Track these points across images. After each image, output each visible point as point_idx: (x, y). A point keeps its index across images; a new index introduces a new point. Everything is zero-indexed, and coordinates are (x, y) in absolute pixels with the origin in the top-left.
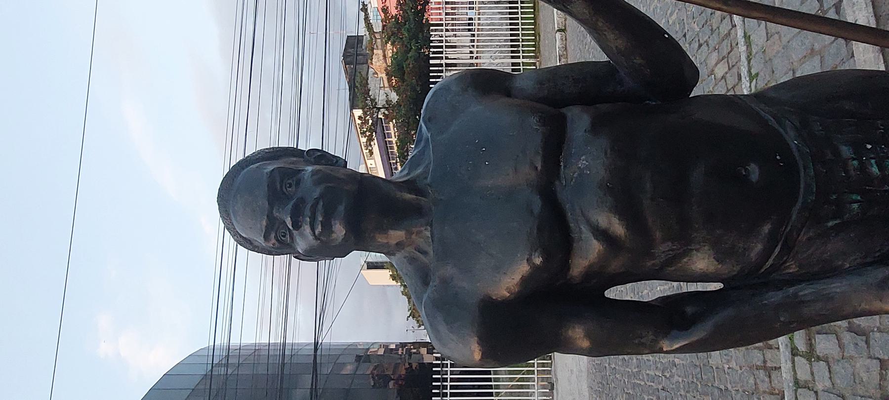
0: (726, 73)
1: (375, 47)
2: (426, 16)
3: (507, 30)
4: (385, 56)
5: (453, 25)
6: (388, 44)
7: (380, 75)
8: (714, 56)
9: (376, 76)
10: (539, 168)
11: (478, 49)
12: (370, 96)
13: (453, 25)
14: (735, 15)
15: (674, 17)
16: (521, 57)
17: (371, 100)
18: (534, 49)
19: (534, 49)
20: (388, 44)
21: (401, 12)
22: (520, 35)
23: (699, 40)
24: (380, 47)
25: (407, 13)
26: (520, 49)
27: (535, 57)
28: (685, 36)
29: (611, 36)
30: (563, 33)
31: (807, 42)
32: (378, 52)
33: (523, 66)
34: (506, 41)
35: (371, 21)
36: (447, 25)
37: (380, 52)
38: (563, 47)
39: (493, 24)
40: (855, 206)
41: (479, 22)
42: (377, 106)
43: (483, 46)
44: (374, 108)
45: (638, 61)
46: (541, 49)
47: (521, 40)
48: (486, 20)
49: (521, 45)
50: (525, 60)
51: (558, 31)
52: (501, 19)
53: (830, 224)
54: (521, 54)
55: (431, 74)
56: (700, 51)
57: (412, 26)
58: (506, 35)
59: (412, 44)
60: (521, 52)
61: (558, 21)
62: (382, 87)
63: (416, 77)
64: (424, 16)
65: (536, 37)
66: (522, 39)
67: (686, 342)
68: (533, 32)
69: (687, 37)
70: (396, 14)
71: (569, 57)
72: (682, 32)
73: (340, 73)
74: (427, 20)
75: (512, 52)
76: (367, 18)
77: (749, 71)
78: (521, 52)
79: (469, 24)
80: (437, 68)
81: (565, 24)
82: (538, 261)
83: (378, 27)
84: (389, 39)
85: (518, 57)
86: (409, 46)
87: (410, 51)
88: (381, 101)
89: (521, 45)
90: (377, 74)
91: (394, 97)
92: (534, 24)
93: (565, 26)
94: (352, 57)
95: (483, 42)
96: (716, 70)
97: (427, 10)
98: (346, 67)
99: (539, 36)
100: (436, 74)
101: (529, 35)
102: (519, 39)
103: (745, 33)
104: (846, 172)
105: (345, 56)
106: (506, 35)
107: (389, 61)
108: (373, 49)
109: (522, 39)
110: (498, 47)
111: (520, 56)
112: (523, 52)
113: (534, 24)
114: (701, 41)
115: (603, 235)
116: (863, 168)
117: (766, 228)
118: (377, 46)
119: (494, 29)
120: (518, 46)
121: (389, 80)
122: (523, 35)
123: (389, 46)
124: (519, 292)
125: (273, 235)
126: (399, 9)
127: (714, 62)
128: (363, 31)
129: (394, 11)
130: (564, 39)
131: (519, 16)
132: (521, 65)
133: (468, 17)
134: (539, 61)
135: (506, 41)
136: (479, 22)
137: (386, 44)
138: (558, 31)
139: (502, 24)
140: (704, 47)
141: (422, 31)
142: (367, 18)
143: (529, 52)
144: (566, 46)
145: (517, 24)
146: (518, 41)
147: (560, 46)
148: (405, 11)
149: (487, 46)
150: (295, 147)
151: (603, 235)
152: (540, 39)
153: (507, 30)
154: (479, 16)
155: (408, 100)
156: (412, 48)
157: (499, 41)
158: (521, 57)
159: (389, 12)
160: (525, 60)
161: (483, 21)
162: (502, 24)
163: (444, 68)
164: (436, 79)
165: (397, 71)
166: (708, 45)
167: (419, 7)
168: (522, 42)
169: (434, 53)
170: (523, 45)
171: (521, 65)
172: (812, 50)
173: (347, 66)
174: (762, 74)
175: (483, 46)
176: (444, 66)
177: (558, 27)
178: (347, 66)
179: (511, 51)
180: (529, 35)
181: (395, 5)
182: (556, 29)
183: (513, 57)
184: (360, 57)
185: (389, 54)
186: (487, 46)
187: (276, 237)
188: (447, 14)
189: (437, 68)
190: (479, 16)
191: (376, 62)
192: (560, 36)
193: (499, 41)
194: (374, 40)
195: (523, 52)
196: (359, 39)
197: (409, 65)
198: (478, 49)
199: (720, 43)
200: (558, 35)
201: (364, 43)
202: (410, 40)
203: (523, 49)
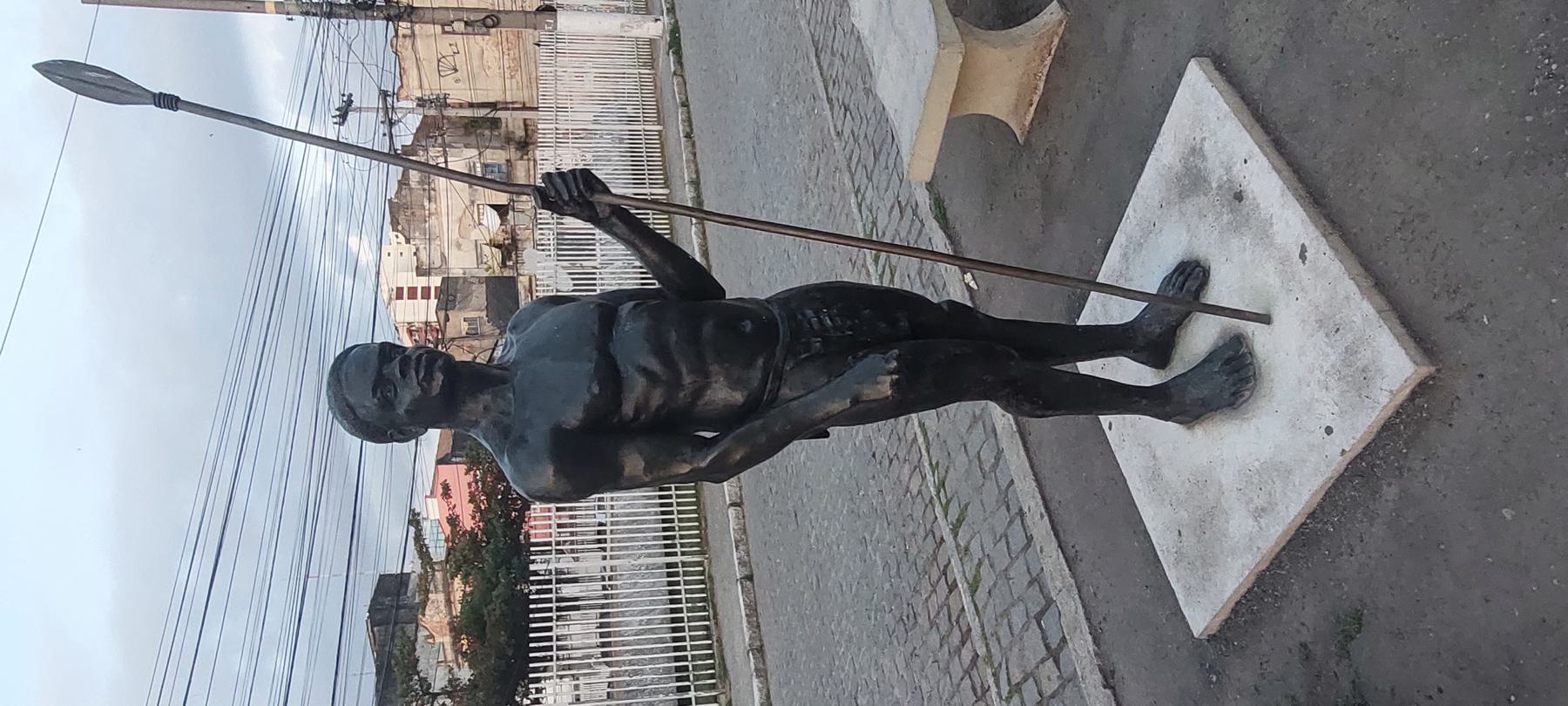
0: (921, 486)
1: (432, 588)
2: (526, 527)
3: (656, 521)
4: (449, 602)
5: (572, 543)
6: (456, 579)
7: (439, 640)
8: (907, 469)
9: (431, 641)
10: (597, 334)
11: (613, 545)
12: (418, 673)
13: (572, 543)
14: (690, 205)
15: (860, 437)
16: (679, 553)
17: (421, 679)
18: (699, 540)
19: (699, 540)
20: (456, 579)
21: (481, 524)
22: (683, 592)
23: (889, 456)
24: (440, 588)
25: (492, 524)
26: (677, 541)
27: (702, 553)
28: (874, 455)
29: (647, 251)
30: (739, 508)
31: (968, 410)
32: (437, 597)
33: (683, 567)
34: (655, 538)
35: (427, 542)
36: (558, 543)
37: (441, 597)
38: (740, 529)
39: (635, 514)
40: (818, 344)
41: (612, 511)
42: (431, 691)
43: (620, 549)
44: (424, 694)
45: (670, 271)
46: (710, 538)
47: (677, 528)
48: (622, 508)
49: (678, 536)
50: (685, 559)
51: (731, 505)
52: (646, 506)
53: (803, 356)
54: (678, 550)
55: (531, 645)
56: (891, 469)
57: (501, 545)
58: (655, 530)
59: (500, 575)
60: (678, 545)
61: (729, 491)
62: (442, 662)
63: (505, 632)
64: (522, 528)
65: (700, 524)
66: (679, 527)
67: (715, 454)
68: (696, 515)
69: (876, 455)
70: (472, 528)
71: (750, 543)
72: (871, 450)
73: (366, 645)
74: (528, 536)
75: (666, 546)
76: (419, 538)
77: (931, 464)
78: (678, 545)
79: (599, 533)
80: (540, 606)
81: (741, 495)
82: (596, 390)
83: (438, 552)
84: (458, 569)
85: (675, 554)
86: (494, 580)
87: (496, 586)
88: (439, 682)
89: (678, 536)
90: (433, 637)
91: (465, 674)
92: (697, 503)
93: (741, 498)
94: (387, 612)
95: (619, 542)
96: (911, 486)
97: (526, 519)
98: (372, 631)
99: (706, 521)
100: (542, 596)
101: (689, 520)
102: (674, 527)
103: (920, 423)
104: (811, 325)
105: (374, 609)
106: (655, 530)
107: (457, 609)
108: (427, 591)
109: (679, 527)
110: (643, 548)
111: (676, 552)
112: (682, 545)
113: (697, 503)
114: (891, 456)
115: (645, 371)
116: (821, 322)
117: (760, 362)
118: (436, 588)
119: (636, 521)
120: (673, 537)
121: (456, 641)
122: (680, 520)
123: (457, 581)
124: (585, 418)
125: (379, 391)
126: (477, 519)
127: (907, 479)
128: (413, 566)
129: (468, 523)
130: (741, 517)
131: (674, 508)
132: (680, 565)
133: (597, 520)
134: (707, 559)
135: (655, 538)
136: (612, 511)
137: (452, 579)
138: (731, 505)
139: (649, 513)
140: (895, 462)
141: (519, 555)
142: (419, 538)
143: (692, 545)
144: (744, 526)
145: (671, 505)
146: (673, 529)
147: (736, 528)
148: (488, 522)
149: (626, 548)
150: (364, 442)
151: (645, 371)
152: (706, 526)
153: (656, 521)
154: (612, 503)
155: (492, 675)
156: (500, 582)
157: (645, 539)
158: (679, 553)
159: (461, 524)
160: (685, 559)
161: (617, 509)
162: (649, 513)
163: (554, 578)
164: (539, 647)
165: (470, 625)
166: (898, 458)
167: (513, 514)
168: (679, 530)
169: (538, 592)
170: (680, 535)
171: (680, 565)
172: (974, 416)
173: (375, 629)
174: (940, 461)
175: (620, 549)
176: (554, 573)
177: (730, 500)
178: (375, 629)
179: (665, 544)
180: (689, 520)
181: (471, 513)
182: (728, 502)
183: (667, 554)
184: (403, 611)
185: (458, 595)
186: (626, 548)
187: (382, 393)
188: (559, 526)
189: (540, 606)
190: (612, 503)
191: (432, 616)
192: (734, 512)
193: (645, 539)
194: (430, 574)
195: (682, 545)
196: (402, 579)
197: (494, 611)
198: (613, 545)
199: (909, 452)
200: (732, 512)
201: (411, 586)
202: (498, 567)
203: (682, 541)
